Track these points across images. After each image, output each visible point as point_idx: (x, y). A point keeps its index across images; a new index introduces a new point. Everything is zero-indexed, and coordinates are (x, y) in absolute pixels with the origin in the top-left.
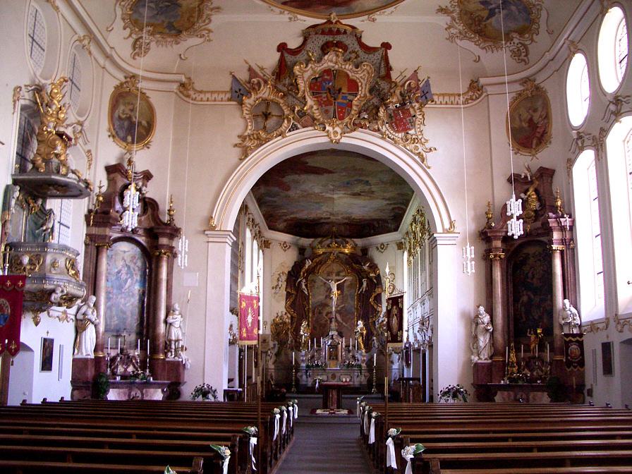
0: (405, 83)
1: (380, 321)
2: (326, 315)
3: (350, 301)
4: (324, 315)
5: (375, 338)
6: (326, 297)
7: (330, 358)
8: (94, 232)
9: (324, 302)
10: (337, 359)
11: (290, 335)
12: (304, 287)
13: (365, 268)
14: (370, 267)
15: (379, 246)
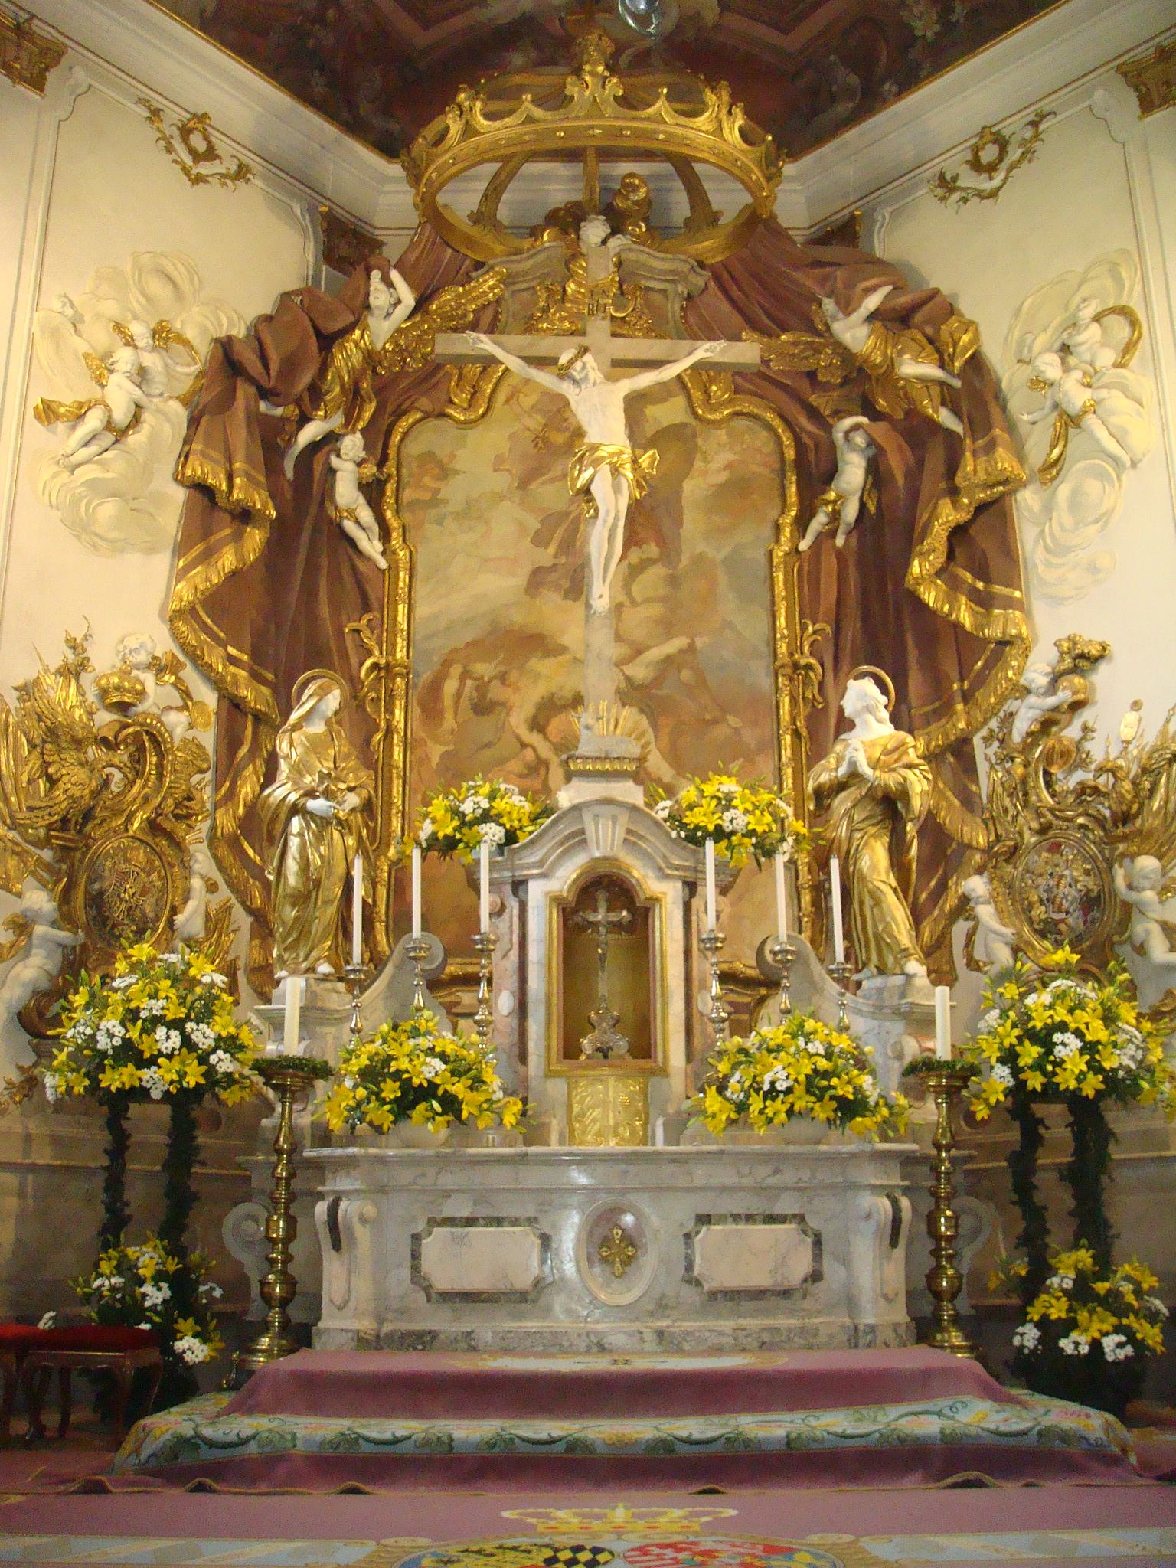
0: (822, 665)
1: (1021, 727)
2: (538, 724)
3: (728, 606)
4: (518, 721)
5: (977, 885)
6: (537, 580)
7: (571, 1050)
8: (132, 1166)
9: (518, 618)
10: (643, 1047)
11: (202, 860)
12: (346, 492)
13: (854, 332)
14: (896, 320)
15: (955, 164)
